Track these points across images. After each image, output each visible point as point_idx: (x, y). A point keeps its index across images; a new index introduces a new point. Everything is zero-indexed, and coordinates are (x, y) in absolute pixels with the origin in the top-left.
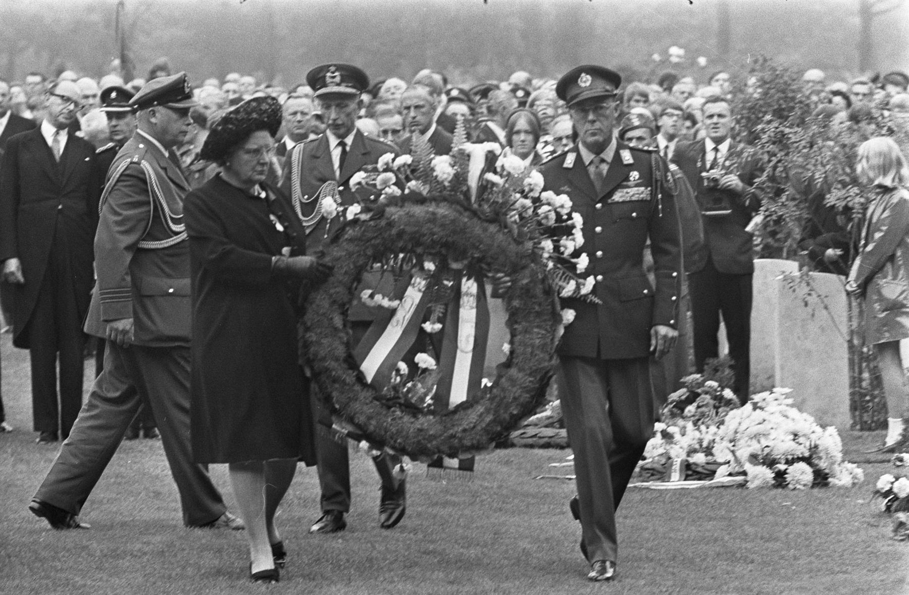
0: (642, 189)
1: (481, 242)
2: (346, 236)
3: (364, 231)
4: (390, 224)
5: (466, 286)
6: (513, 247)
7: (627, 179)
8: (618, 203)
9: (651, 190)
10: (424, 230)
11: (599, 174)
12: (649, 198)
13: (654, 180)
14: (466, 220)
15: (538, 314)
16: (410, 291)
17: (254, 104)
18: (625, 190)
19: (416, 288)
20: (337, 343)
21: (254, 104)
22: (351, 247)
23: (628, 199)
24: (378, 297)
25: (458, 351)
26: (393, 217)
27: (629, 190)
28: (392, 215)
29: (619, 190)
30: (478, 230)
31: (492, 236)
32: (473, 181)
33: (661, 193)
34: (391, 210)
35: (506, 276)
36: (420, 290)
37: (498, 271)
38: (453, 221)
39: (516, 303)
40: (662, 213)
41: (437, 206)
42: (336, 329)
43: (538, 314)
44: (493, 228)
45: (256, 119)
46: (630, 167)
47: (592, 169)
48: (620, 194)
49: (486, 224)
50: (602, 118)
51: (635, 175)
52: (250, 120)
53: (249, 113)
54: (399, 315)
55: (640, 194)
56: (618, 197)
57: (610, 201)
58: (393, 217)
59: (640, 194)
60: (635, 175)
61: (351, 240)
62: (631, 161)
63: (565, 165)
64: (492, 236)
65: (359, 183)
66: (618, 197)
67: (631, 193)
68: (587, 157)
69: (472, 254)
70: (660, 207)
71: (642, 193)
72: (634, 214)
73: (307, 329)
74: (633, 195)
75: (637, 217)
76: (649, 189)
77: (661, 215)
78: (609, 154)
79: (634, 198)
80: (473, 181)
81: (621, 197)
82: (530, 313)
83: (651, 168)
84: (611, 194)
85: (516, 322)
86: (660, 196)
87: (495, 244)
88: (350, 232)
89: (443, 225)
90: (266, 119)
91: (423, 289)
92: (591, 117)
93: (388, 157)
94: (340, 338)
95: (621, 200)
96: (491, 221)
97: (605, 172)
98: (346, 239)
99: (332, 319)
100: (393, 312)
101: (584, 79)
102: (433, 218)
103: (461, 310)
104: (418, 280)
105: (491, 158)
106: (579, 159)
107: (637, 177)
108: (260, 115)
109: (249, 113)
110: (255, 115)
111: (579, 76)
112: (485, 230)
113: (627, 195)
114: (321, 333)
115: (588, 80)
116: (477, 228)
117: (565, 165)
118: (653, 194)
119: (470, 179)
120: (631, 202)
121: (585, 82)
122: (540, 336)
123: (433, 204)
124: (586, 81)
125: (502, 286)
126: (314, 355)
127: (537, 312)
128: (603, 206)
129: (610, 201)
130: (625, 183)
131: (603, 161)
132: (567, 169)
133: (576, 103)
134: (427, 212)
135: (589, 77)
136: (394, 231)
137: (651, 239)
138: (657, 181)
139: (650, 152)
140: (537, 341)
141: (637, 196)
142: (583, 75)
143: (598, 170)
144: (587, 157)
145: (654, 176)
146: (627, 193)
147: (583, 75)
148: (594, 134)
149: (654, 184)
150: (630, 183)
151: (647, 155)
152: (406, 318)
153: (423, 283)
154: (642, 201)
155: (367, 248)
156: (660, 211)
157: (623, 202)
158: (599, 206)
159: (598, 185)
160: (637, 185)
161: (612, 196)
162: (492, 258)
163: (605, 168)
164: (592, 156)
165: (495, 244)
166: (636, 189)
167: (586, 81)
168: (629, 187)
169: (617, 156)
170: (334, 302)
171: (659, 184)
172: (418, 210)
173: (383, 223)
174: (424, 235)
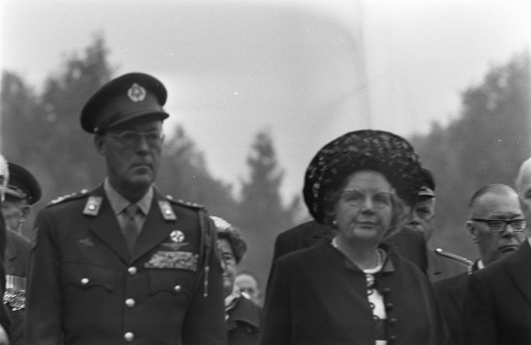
0: (189, 254)
8: (157, 269)
9: (198, 259)
11: (131, 228)
12: (195, 269)
13: (202, 246)
18: (167, 254)
23: (171, 266)
27: (172, 254)
29: (160, 252)
33: (209, 265)
40: (209, 293)
46: (172, 225)
48: (161, 258)
51: (177, 236)
55: (186, 261)
57: (147, 265)
59: (186, 261)
62: (173, 217)
67: (175, 259)
70: (206, 283)
71: (189, 260)
72: (177, 287)
74: (178, 261)
75: (181, 292)
76: (197, 256)
77: (206, 295)
78: (146, 204)
79: (178, 266)
81: (162, 262)
83: (199, 228)
84: (148, 256)
86: (207, 268)
95: (162, 266)
101: (137, 92)
106: (105, 207)
107: (182, 238)
111: (129, 87)
113: (169, 260)
115: (141, 93)
117: (86, 211)
118: (201, 264)
120: (174, 270)
129: (147, 265)
130: (166, 245)
131: (139, 212)
132: (89, 217)
135: (143, 91)
137: (336, 250)
138: (205, 247)
139: (196, 209)
141: (183, 263)
142: (135, 85)
145: (202, 239)
146: (170, 257)
147: (135, 85)
149: (202, 251)
150: (172, 245)
151: (192, 213)
156: (206, 290)
157: (165, 269)
160: (182, 249)
161: (150, 259)
163: (139, 222)
164: (126, 204)
166: (181, 253)
168: (170, 250)
169: (155, 206)
171: (208, 252)
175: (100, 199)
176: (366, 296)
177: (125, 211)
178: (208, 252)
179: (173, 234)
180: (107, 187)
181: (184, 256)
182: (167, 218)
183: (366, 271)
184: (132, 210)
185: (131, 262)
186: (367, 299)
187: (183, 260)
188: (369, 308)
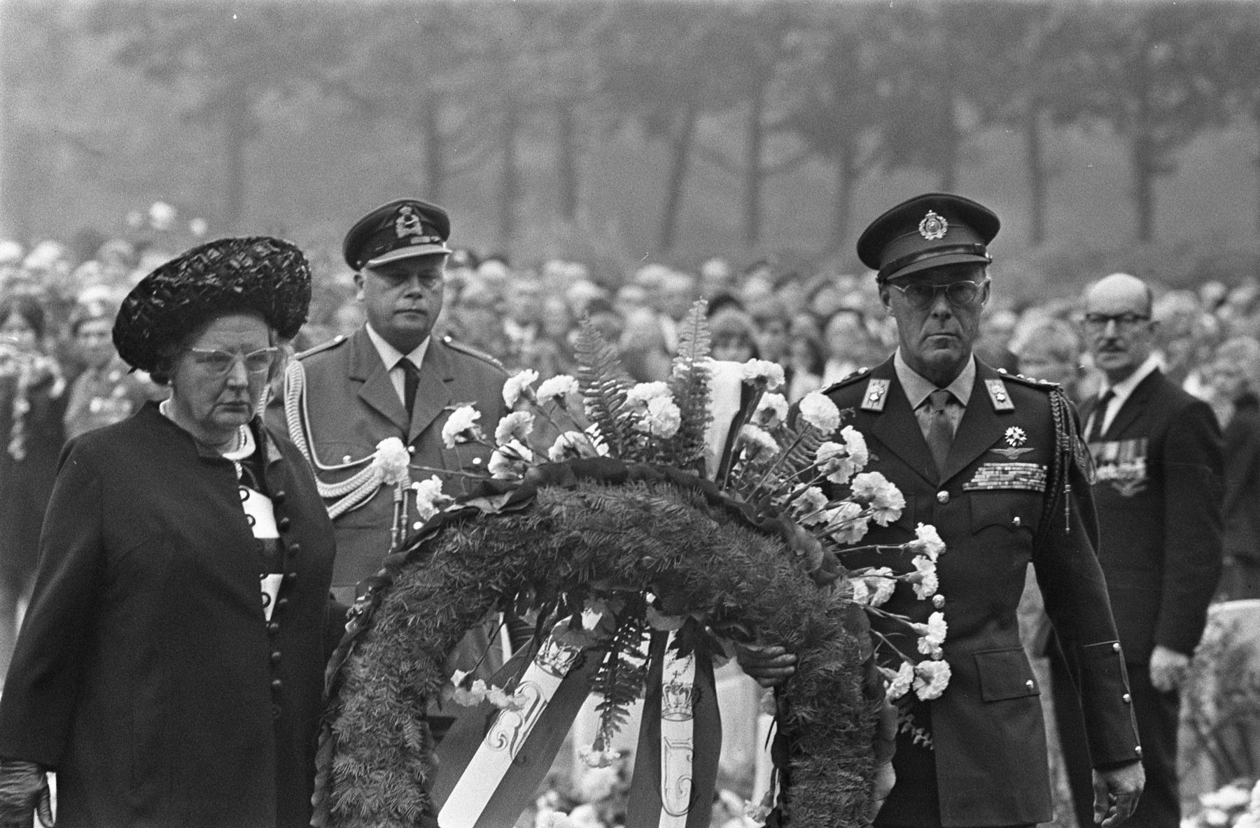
1: (743, 576)
2: (449, 547)
3: (489, 538)
4: (548, 526)
5: (673, 669)
6: (809, 590)
7: (1002, 442)
8: (985, 491)
10: (624, 543)
11: (943, 428)
14: (714, 525)
15: (852, 738)
16: (533, 673)
17: (214, 254)
18: (999, 466)
19: (548, 668)
20: (404, 785)
21: (214, 254)
22: (457, 573)
24: (478, 686)
25: (663, 813)
26: (556, 511)
27: (1007, 466)
28: (551, 508)
30: (737, 549)
31: (767, 567)
32: (714, 439)
34: (548, 495)
35: (787, 652)
36: (556, 673)
37: (771, 641)
38: (687, 528)
39: (804, 712)
41: (653, 492)
42: (404, 750)
43: (852, 738)
44: (770, 547)
45: (212, 287)
47: (926, 418)
49: (756, 538)
50: (963, 312)
52: (198, 289)
53: (198, 275)
54: (507, 723)
56: (983, 478)
57: (967, 486)
58: (556, 511)
60: (1014, 433)
61: (456, 557)
62: (1009, 405)
63: (866, 405)
64: (767, 567)
65: (466, 433)
66: (983, 478)
67: (1012, 474)
68: (915, 389)
69: (722, 599)
70: (1067, 509)
71: (1034, 474)
72: (1017, 519)
73: (338, 748)
77: (1068, 529)
78: (963, 386)
79: (1017, 485)
80: (714, 439)
81: (991, 479)
82: (833, 734)
85: (798, 754)
87: (775, 582)
88: (458, 537)
89: (664, 535)
90: (239, 290)
91: (563, 671)
92: (941, 306)
93: (521, 379)
94: (412, 771)
96: (767, 532)
97: (955, 424)
98: (449, 553)
99: (399, 728)
100: (490, 714)
102: (644, 518)
103: (664, 724)
104: (554, 649)
105: (750, 392)
108: (225, 279)
109: (198, 275)
110: (211, 279)
112: (754, 550)
114: (372, 759)
116: (735, 546)
117: (866, 405)
119: (707, 437)
121: (934, 230)
122: (850, 787)
123: (643, 484)
124: (933, 228)
125: (771, 671)
126: (350, 805)
127: (849, 734)
128: (951, 496)
129: (967, 486)
131: (952, 400)
133: (910, 275)
134: (631, 503)
136: (556, 542)
137: (165, 420)
139: (1046, 389)
140: (845, 798)
143: (942, 419)
144: (915, 389)
148: (942, 344)
150: (1009, 452)
151: (1039, 396)
152: (522, 730)
153: (565, 656)
154: (1030, 492)
155: (492, 574)
157: (996, 491)
158: (943, 494)
159: (940, 455)
160: (1021, 458)
162: (762, 611)
163: (955, 415)
164: (929, 390)
165: (775, 582)
167: (933, 228)
170: (407, 692)
172: (611, 499)
173: (533, 521)
174: (622, 553)
175: (886, 383)
176: (239, 503)
177: (928, 402)
178: (1067, 460)
179: (1009, 432)
180: (899, 364)
181: (1025, 469)
182: (999, 406)
183: (229, 456)
184: (940, 398)
185: (942, 482)
186: (242, 508)
187: (1025, 476)
188: (245, 524)
